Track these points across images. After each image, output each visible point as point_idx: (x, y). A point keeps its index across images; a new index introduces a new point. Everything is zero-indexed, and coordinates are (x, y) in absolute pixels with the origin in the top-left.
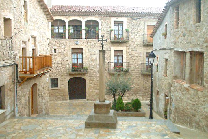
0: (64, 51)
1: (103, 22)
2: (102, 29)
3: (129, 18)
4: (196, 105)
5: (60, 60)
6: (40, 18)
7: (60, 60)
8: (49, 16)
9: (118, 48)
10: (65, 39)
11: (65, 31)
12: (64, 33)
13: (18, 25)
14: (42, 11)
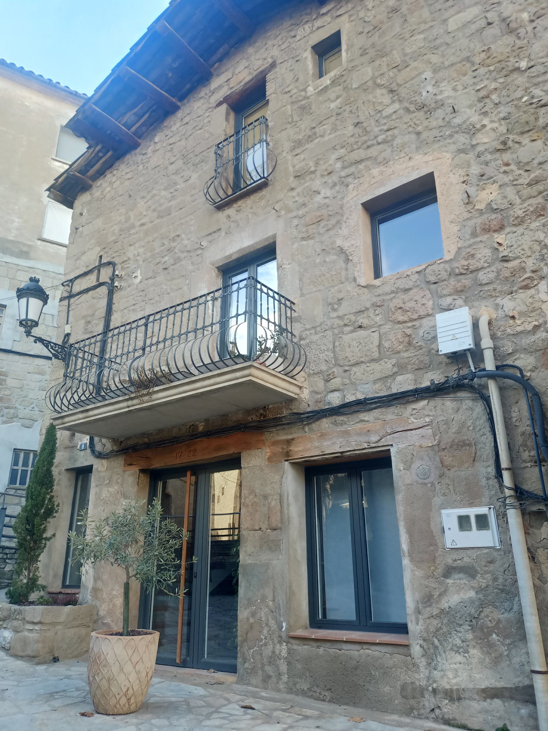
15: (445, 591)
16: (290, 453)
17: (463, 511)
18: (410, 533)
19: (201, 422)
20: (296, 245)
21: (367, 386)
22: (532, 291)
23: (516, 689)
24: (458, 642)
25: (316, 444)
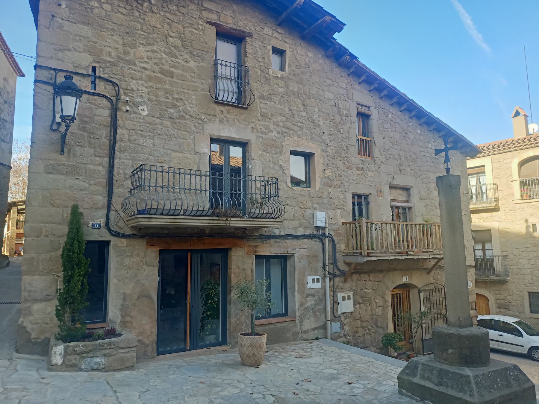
15: (307, 302)
16: (257, 251)
17: (314, 277)
18: (298, 284)
19: (208, 228)
20: (260, 152)
21: (289, 229)
22: (335, 211)
23: (320, 326)
24: (309, 316)
25: (268, 249)
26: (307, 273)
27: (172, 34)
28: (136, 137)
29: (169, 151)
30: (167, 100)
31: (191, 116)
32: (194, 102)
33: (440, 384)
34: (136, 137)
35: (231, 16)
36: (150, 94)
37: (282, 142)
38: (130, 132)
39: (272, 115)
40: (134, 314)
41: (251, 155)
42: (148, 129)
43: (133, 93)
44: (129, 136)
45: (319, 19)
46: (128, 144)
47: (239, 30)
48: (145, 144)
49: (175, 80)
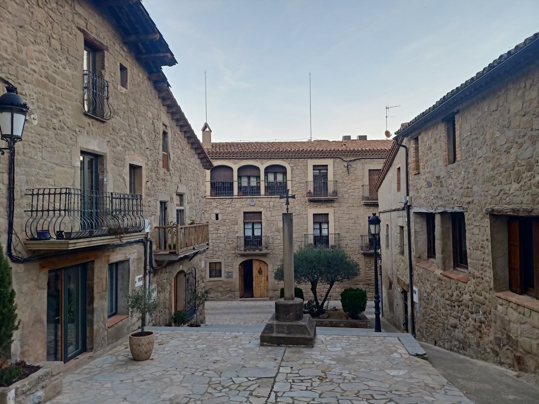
0: (231, 217)
1: (295, 168)
2: (293, 179)
3: (338, 160)
4: (456, 307)
5: (225, 232)
6: (189, 163)
7: (225, 232)
8: (205, 160)
9: (321, 210)
10: (232, 197)
11: (258, 183)
12: (259, 188)
13: (154, 175)
14: (193, 152)
26: (135, 274)
27: (54, 36)
28: (29, 150)
29: (54, 165)
30: (51, 109)
31: (68, 127)
32: (70, 113)
33: (290, 333)
34: (29, 150)
35: (94, 26)
36: (39, 100)
37: (125, 155)
38: (24, 144)
39: (119, 130)
40: (30, 342)
41: (106, 169)
42: (37, 140)
43: (26, 98)
44: (24, 147)
45: (159, 52)
46: (23, 157)
47: (100, 42)
48: (36, 158)
49: (56, 87)
